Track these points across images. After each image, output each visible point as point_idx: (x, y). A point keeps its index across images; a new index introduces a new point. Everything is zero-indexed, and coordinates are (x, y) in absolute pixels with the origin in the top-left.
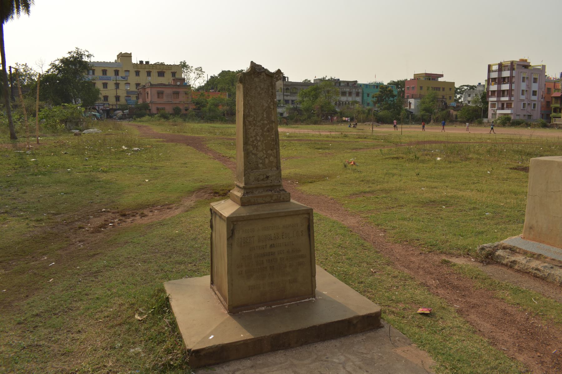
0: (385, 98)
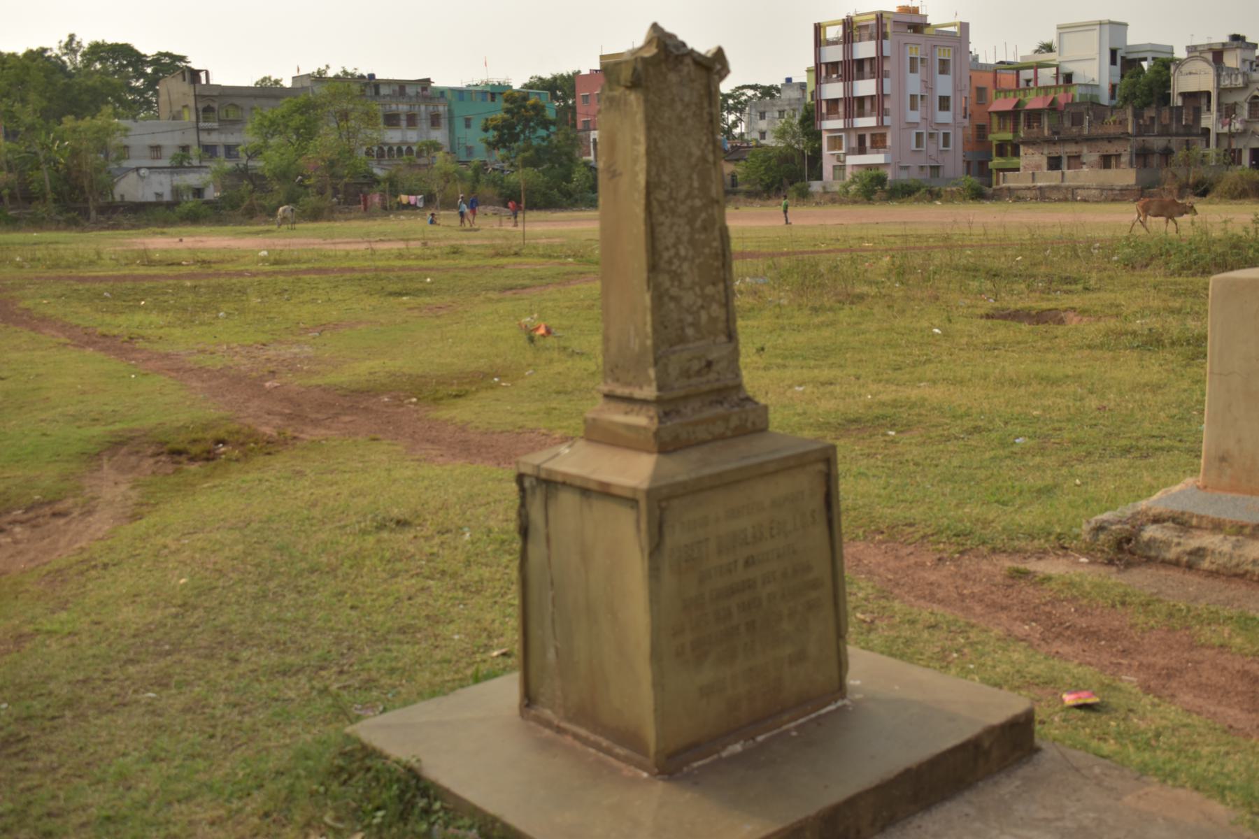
0: (523, 131)
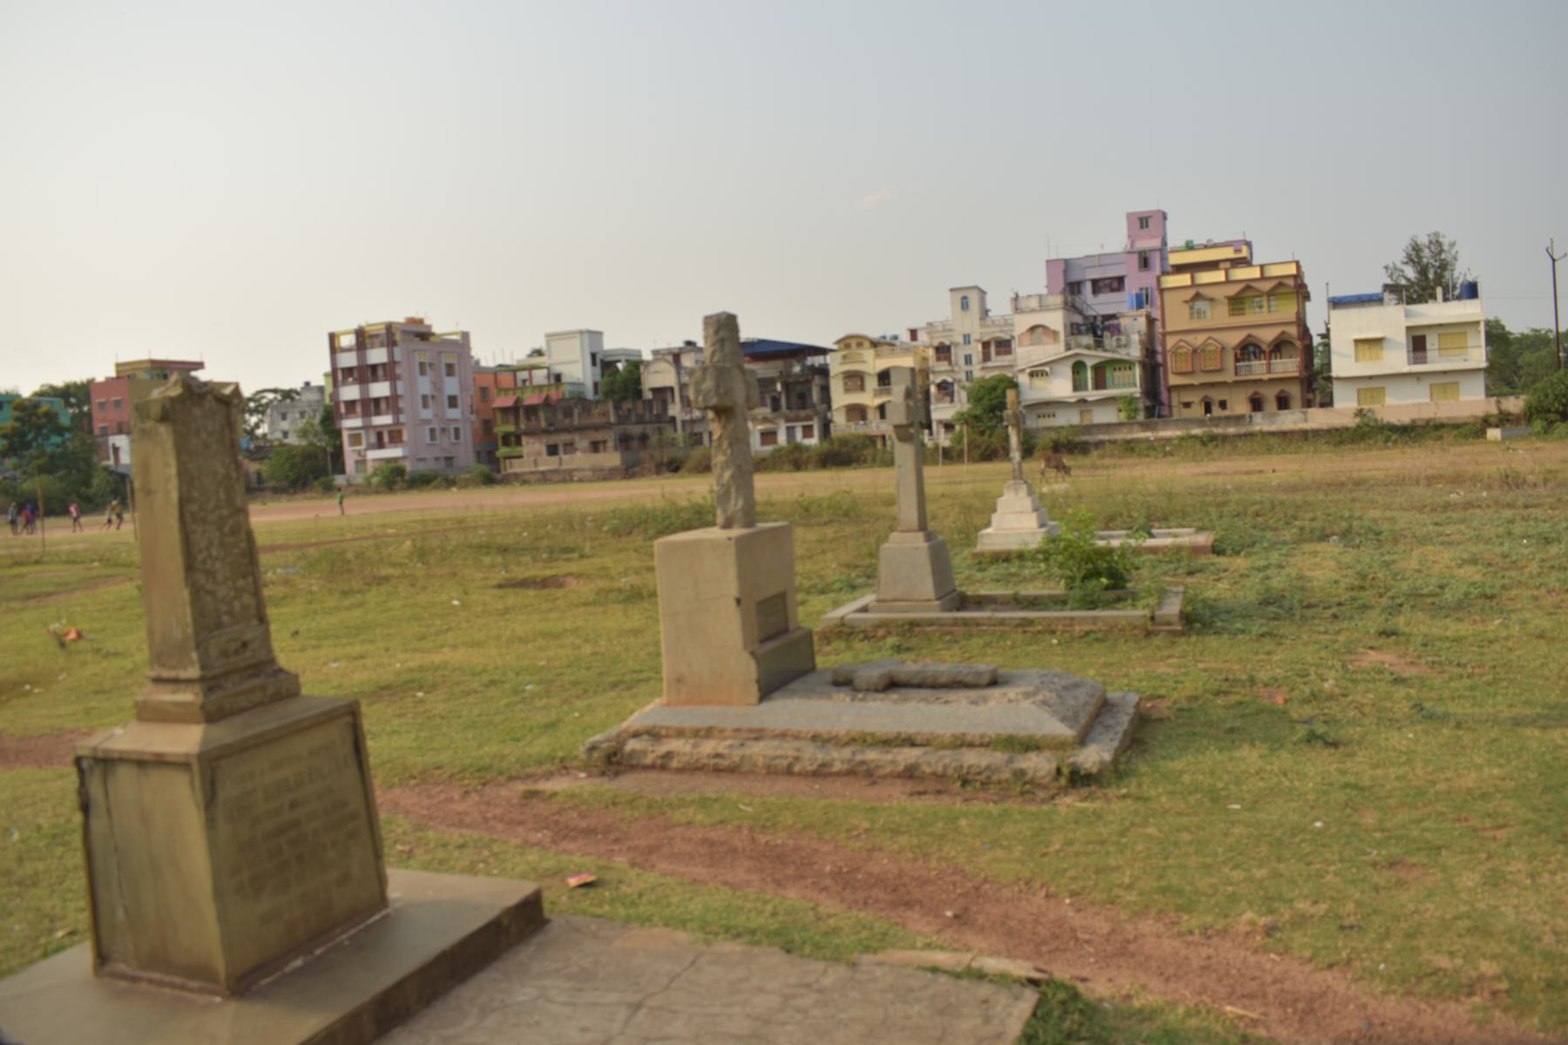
0: (35, 439)
